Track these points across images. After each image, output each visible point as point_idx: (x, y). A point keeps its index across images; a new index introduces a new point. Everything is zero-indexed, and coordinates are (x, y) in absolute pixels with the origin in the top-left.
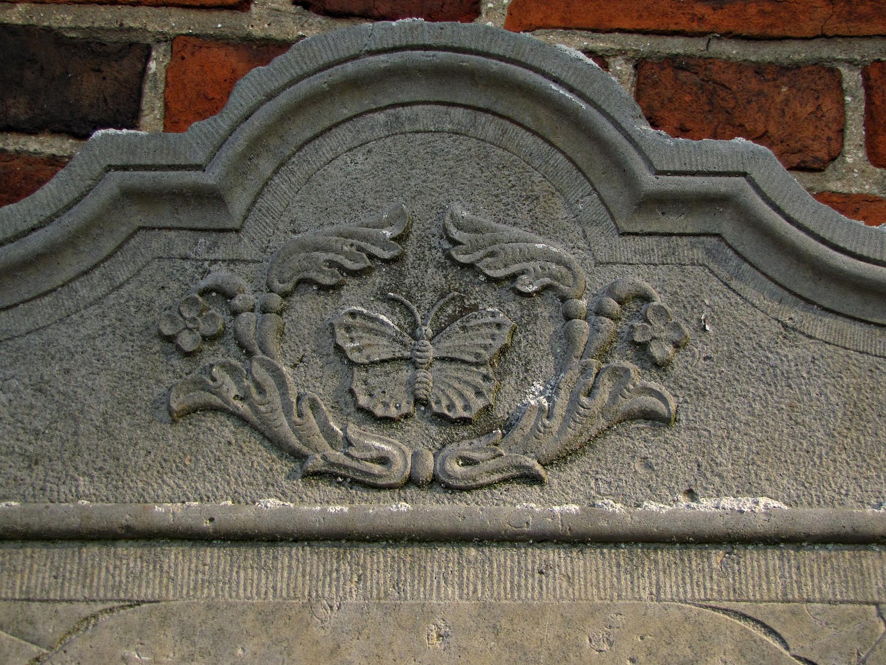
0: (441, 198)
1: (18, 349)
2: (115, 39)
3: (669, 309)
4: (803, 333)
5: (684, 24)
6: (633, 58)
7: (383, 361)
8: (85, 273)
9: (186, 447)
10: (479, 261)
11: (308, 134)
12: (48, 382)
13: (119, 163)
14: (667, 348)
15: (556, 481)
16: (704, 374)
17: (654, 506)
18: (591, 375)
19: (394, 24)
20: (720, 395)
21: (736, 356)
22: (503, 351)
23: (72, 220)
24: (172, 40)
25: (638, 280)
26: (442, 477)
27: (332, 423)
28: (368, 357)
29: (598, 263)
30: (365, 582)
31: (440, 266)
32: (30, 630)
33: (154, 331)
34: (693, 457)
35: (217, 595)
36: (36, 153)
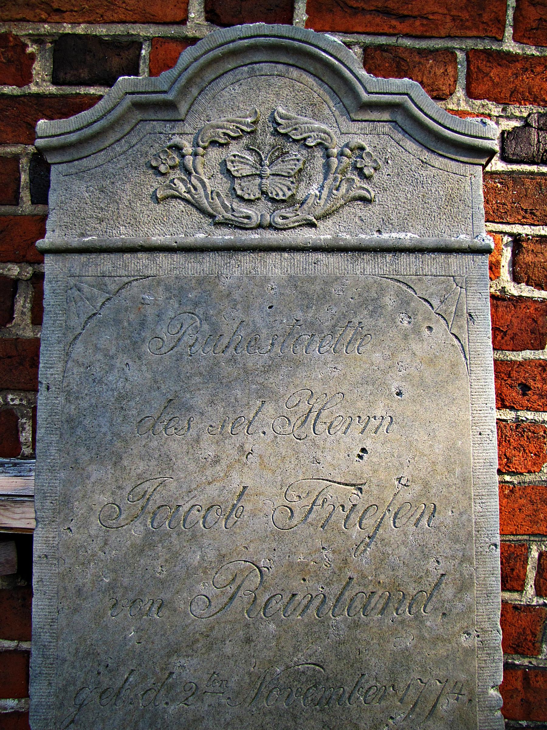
0: (273, 105)
1: (92, 174)
2: (126, 40)
3: (372, 154)
4: (430, 165)
5: (386, 30)
6: (363, 46)
7: (247, 176)
8: (118, 141)
9: (164, 214)
10: (289, 132)
11: (213, 77)
12: (105, 188)
13: (130, 91)
14: (371, 170)
15: (322, 226)
16: (387, 181)
17: (363, 236)
18: (337, 181)
19: (251, 25)
20: (393, 191)
21: (401, 174)
22: (300, 171)
23: (111, 117)
24: (151, 40)
25: (359, 141)
26: (273, 224)
27: (226, 202)
28: (241, 174)
29: (342, 134)
30: (241, 267)
31: (272, 134)
32: (105, 288)
33: (148, 165)
34: (381, 216)
35: (180, 273)
36: (93, 94)
